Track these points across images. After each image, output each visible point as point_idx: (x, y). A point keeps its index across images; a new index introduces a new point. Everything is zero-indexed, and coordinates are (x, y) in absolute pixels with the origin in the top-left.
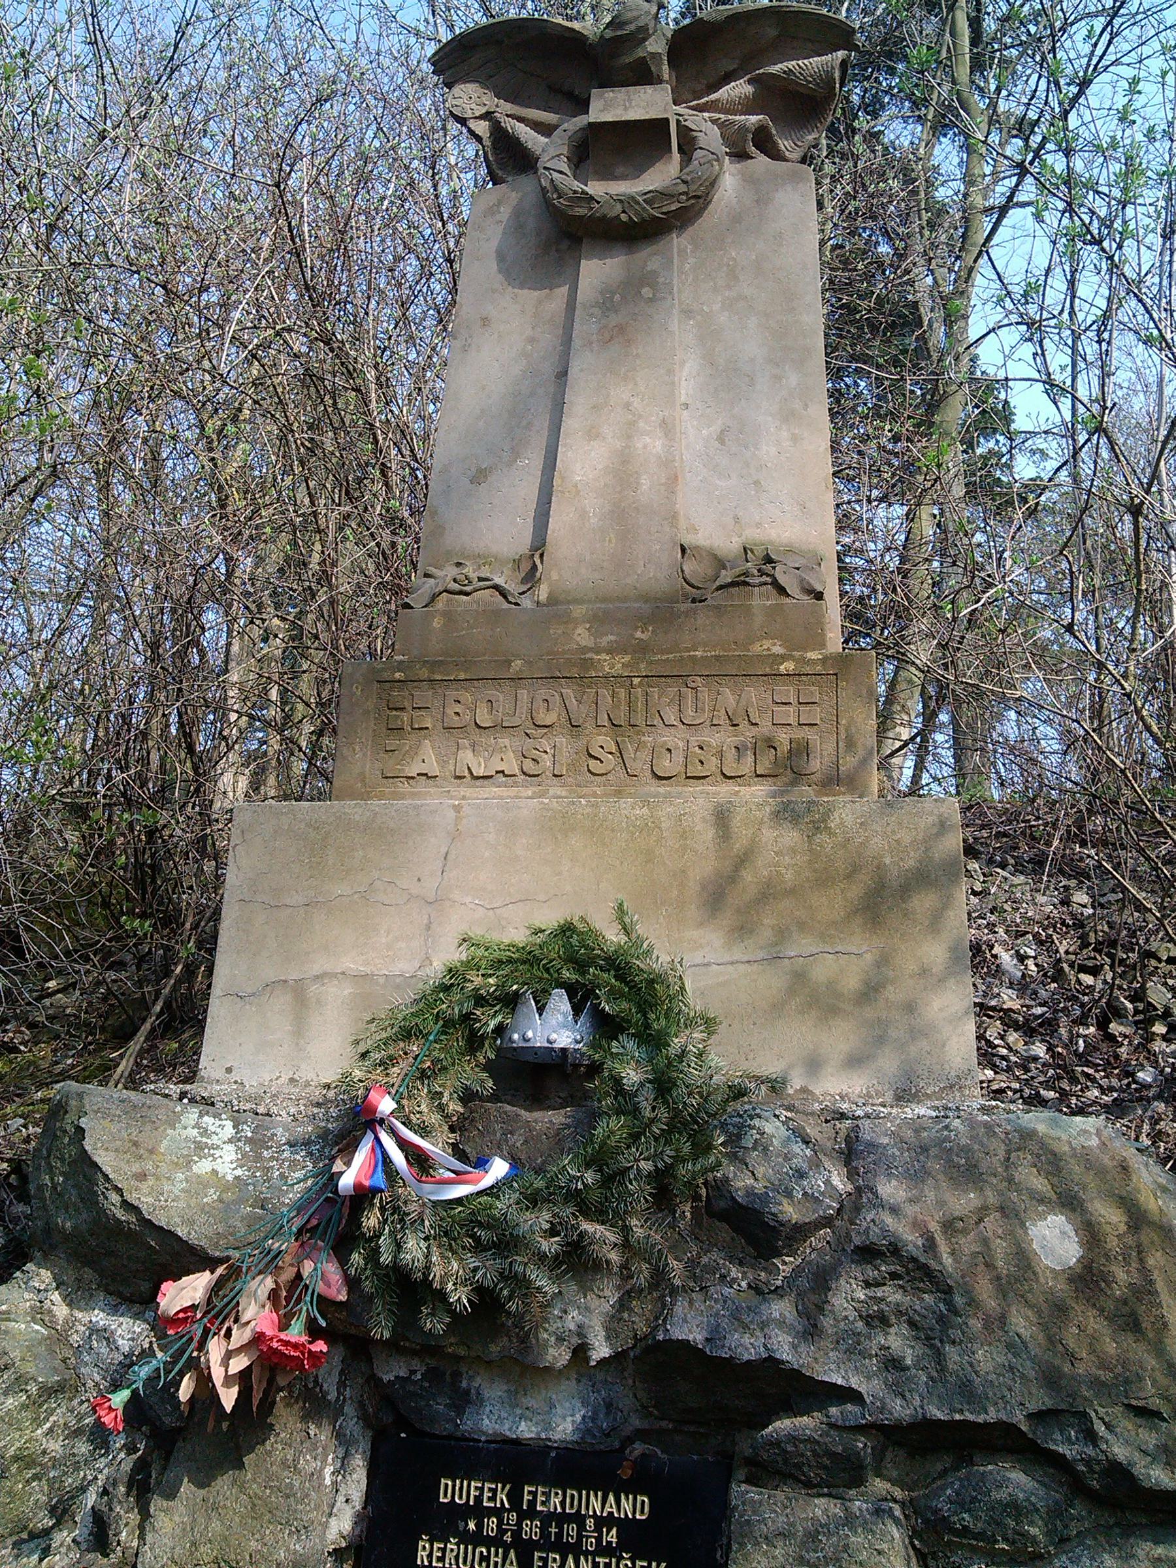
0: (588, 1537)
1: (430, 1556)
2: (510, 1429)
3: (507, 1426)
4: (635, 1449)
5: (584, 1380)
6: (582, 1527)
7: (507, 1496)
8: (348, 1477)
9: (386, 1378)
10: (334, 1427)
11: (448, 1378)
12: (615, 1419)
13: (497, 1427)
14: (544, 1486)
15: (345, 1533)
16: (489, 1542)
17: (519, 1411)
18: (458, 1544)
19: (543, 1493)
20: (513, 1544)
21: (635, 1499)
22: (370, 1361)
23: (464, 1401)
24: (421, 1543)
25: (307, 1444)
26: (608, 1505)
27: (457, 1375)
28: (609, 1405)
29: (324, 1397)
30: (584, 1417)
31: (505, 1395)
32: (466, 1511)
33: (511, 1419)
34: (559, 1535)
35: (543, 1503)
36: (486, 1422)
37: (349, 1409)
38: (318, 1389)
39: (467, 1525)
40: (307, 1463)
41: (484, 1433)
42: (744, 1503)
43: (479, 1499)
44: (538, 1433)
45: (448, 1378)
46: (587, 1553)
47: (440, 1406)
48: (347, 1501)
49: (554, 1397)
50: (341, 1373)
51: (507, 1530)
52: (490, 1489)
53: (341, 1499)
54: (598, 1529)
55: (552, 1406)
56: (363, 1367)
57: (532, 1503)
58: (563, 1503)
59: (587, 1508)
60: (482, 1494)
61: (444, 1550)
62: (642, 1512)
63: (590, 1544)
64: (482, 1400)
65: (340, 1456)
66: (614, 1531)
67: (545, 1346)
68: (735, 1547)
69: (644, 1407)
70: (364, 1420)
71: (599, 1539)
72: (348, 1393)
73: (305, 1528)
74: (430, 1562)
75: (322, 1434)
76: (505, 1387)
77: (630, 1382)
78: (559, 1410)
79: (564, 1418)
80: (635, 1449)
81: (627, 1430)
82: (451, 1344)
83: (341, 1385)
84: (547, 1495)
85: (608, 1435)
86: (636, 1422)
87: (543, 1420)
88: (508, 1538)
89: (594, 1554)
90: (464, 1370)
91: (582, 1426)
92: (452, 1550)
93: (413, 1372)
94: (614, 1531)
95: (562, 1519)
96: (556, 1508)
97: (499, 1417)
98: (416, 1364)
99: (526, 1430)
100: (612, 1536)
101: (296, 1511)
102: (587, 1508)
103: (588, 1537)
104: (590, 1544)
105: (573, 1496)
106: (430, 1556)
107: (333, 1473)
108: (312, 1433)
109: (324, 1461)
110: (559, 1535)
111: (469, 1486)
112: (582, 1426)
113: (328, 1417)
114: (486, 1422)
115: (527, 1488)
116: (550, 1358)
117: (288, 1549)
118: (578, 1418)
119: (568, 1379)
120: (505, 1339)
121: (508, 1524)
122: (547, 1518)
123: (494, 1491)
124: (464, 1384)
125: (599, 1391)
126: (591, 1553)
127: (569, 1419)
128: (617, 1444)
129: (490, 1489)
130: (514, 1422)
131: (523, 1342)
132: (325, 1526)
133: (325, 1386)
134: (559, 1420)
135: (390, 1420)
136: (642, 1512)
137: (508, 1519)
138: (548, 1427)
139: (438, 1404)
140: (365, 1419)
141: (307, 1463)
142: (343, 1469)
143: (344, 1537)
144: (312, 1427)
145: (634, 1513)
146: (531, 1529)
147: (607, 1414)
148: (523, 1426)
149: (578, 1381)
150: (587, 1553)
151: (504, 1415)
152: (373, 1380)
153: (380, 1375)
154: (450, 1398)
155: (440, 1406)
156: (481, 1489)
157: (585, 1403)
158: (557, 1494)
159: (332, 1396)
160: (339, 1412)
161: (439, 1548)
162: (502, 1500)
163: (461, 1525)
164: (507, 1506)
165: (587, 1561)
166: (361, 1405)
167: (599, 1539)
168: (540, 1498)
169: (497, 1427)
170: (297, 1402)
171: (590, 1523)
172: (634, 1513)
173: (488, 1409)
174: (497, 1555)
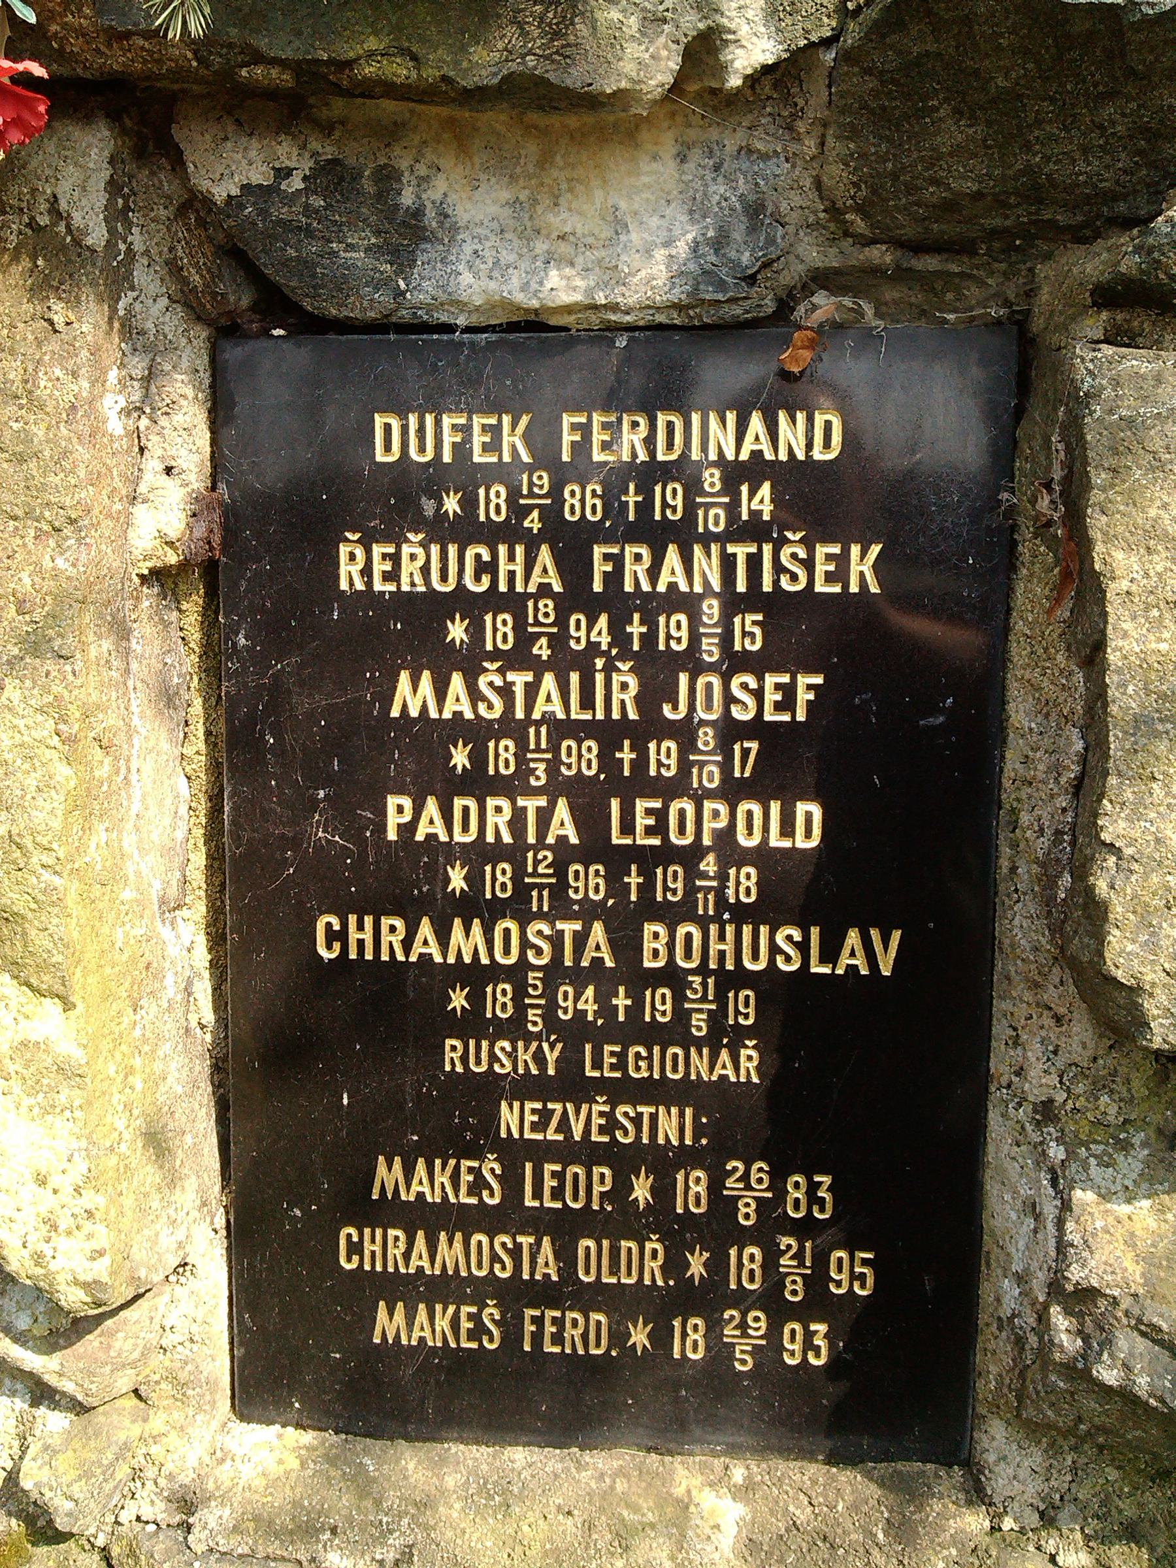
0: (708, 506)
1: (367, 572)
2: (524, 288)
3: (515, 282)
4: (815, 307)
5: (696, 155)
6: (693, 487)
7: (527, 437)
8: (163, 421)
9: (220, 193)
10: (114, 310)
11: (368, 186)
12: (771, 241)
13: (493, 285)
14: (606, 409)
15: (173, 535)
16: (492, 534)
17: (541, 247)
18: (424, 545)
19: (605, 426)
20: (544, 536)
21: (810, 420)
22: (178, 162)
23: (407, 236)
24: (344, 550)
25: (53, 345)
26: (537, 570)
27: (388, 178)
28: (755, 211)
29: (77, 243)
30: (695, 248)
31: (508, 211)
32: (435, 479)
33: (523, 266)
34: (645, 508)
35: (605, 446)
36: (467, 278)
37: (141, 275)
38: (62, 228)
39: (441, 504)
40: (58, 385)
41: (461, 305)
42: (1116, 383)
43: (462, 450)
44: (589, 292)
45: (368, 186)
46: (707, 539)
47: (356, 252)
48: (168, 470)
49: (623, 205)
50: (113, 187)
51: (529, 509)
52: (485, 428)
53: (152, 465)
54: (730, 486)
55: (620, 226)
56: (168, 184)
57: (582, 448)
58: (650, 442)
59: (704, 449)
60: (468, 439)
61: (396, 559)
62: (827, 444)
63: (714, 520)
64: (454, 229)
65: (138, 373)
66: (766, 489)
67: (616, 41)
68: (1099, 478)
69: (834, 212)
70: (187, 305)
71: (732, 509)
72: (137, 239)
73: (72, 521)
74: (369, 584)
75: (87, 322)
76: (505, 195)
77: (810, 146)
78: (635, 237)
79: (648, 253)
80: (815, 307)
81: (791, 273)
82: (371, 54)
83: (117, 217)
84: (614, 428)
85: (751, 280)
86: (812, 253)
87: (599, 261)
88: (533, 522)
89: (724, 538)
90: (404, 164)
91: (692, 266)
92: (413, 557)
93: (284, 173)
94: (766, 489)
95: (650, 474)
96: (634, 455)
97: (496, 263)
98: (286, 152)
99: (562, 288)
100: (761, 501)
101: (43, 488)
102: (704, 449)
103: (708, 506)
104: (714, 520)
105: (670, 426)
106: (367, 572)
107: (126, 412)
108: (59, 320)
109: (98, 380)
110: (645, 508)
111: (438, 423)
112: (692, 266)
113: (93, 284)
114: (467, 278)
115: (567, 420)
116: (629, 67)
117: (38, 570)
118: (682, 248)
119: (655, 158)
120: (511, 31)
121: (531, 495)
122: (616, 479)
123: (496, 430)
124: (407, 198)
125: (730, 180)
126: (716, 538)
127: (660, 254)
128: (770, 306)
129: (485, 428)
130: (534, 272)
131: (556, 35)
132: (126, 522)
133: (77, 219)
134: (636, 259)
135: (245, 302)
136: (827, 444)
137: (531, 484)
138: (613, 274)
139: (351, 247)
140: (189, 302)
141: (58, 385)
142: (147, 403)
143: (170, 544)
144: (58, 306)
145: (809, 446)
146: (582, 502)
147: (752, 229)
148: (554, 279)
149: (682, 158)
150: (707, 539)
151: (507, 257)
152: (194, 205)
153: (204, 185)
154: (377, 233)
155: (356, 252)
156: (466, 429)
157: (697, 210)
158: (635, 425)
159: (97, 236)
160: (117, 281)
161: (385, 556)
162: (514, 447)
163: (429, 506)
164: (526, 458)
165: (708, 554)
166: (174, 268)
167: (732, 509)
168: (598, 437)
169: (493, 285)
170: (15, 258)
171: (712, 479)
172: (809, 446)
173: (468, 249)
174: (511, 558)
